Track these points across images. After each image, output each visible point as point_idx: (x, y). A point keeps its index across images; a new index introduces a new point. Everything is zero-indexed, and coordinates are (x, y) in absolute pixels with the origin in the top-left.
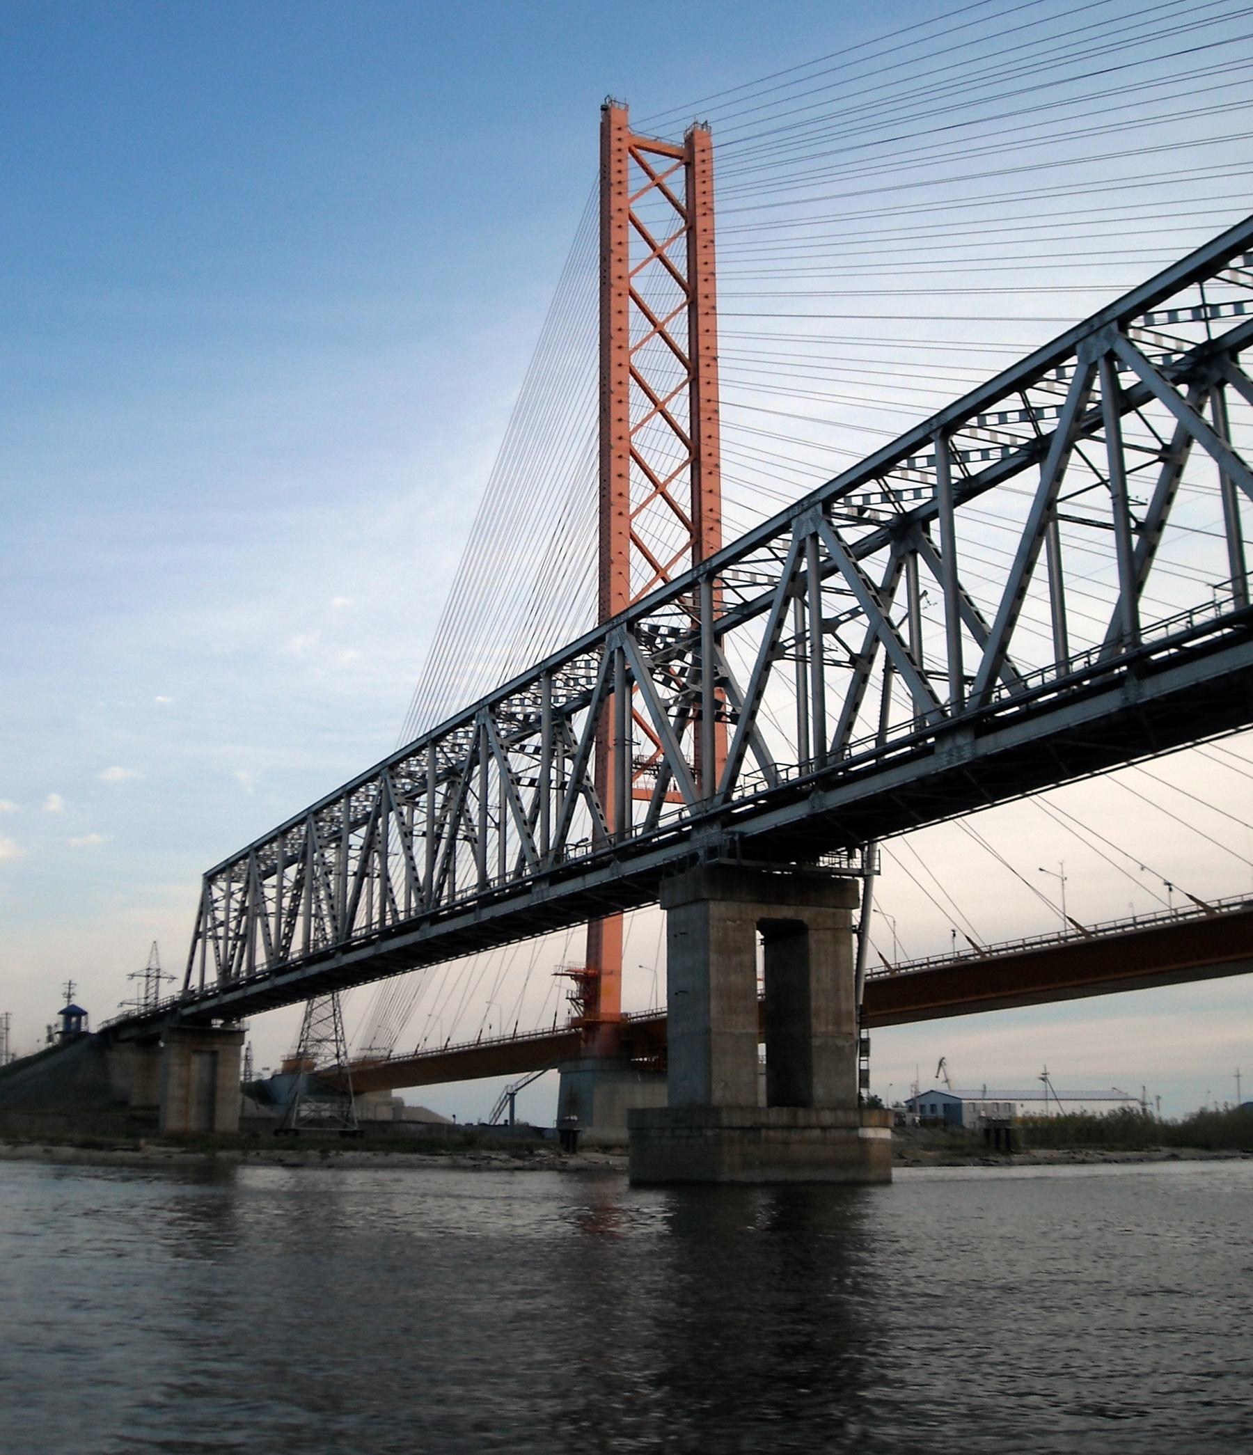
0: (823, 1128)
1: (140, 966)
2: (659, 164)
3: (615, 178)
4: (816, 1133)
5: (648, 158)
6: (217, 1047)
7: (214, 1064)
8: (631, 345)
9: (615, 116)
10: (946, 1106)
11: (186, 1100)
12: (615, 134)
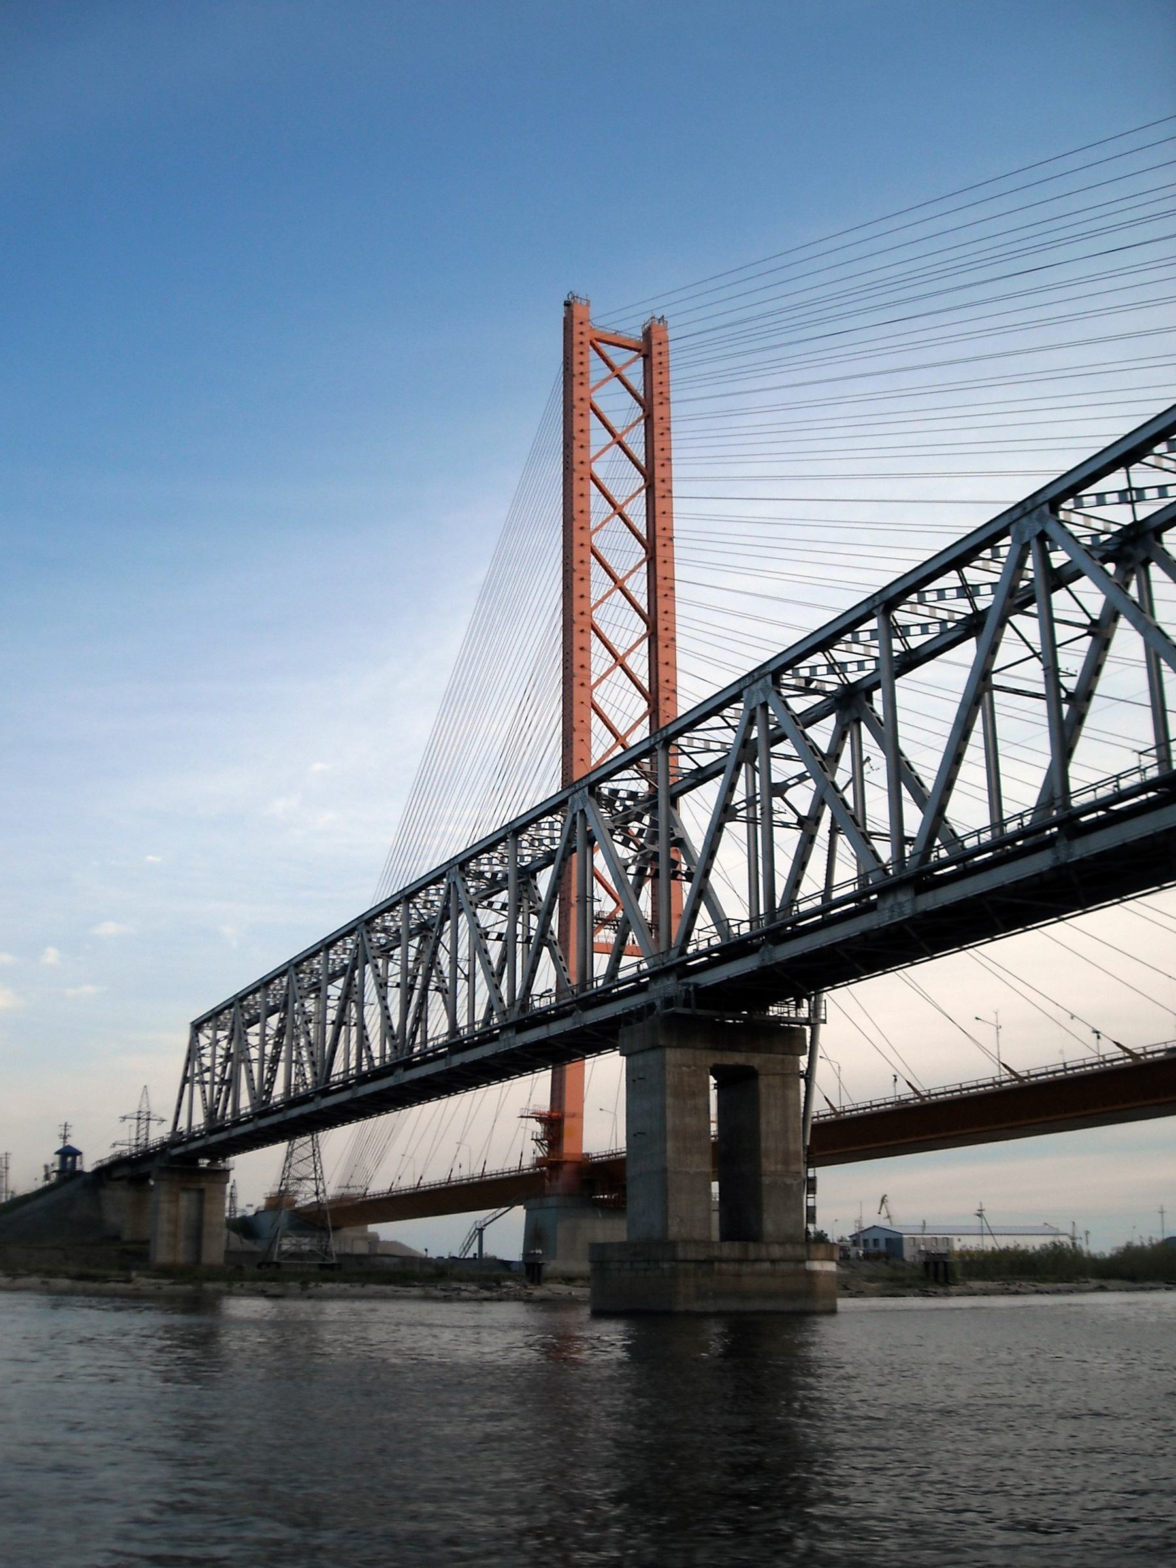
0: (773, 1261)
1: (132, 1109)
2: (619, 357)
4: (766, 1266)
6: (204, 1185)
7: (201, 1202)
8: (593, 526)
10: (888, 1240)
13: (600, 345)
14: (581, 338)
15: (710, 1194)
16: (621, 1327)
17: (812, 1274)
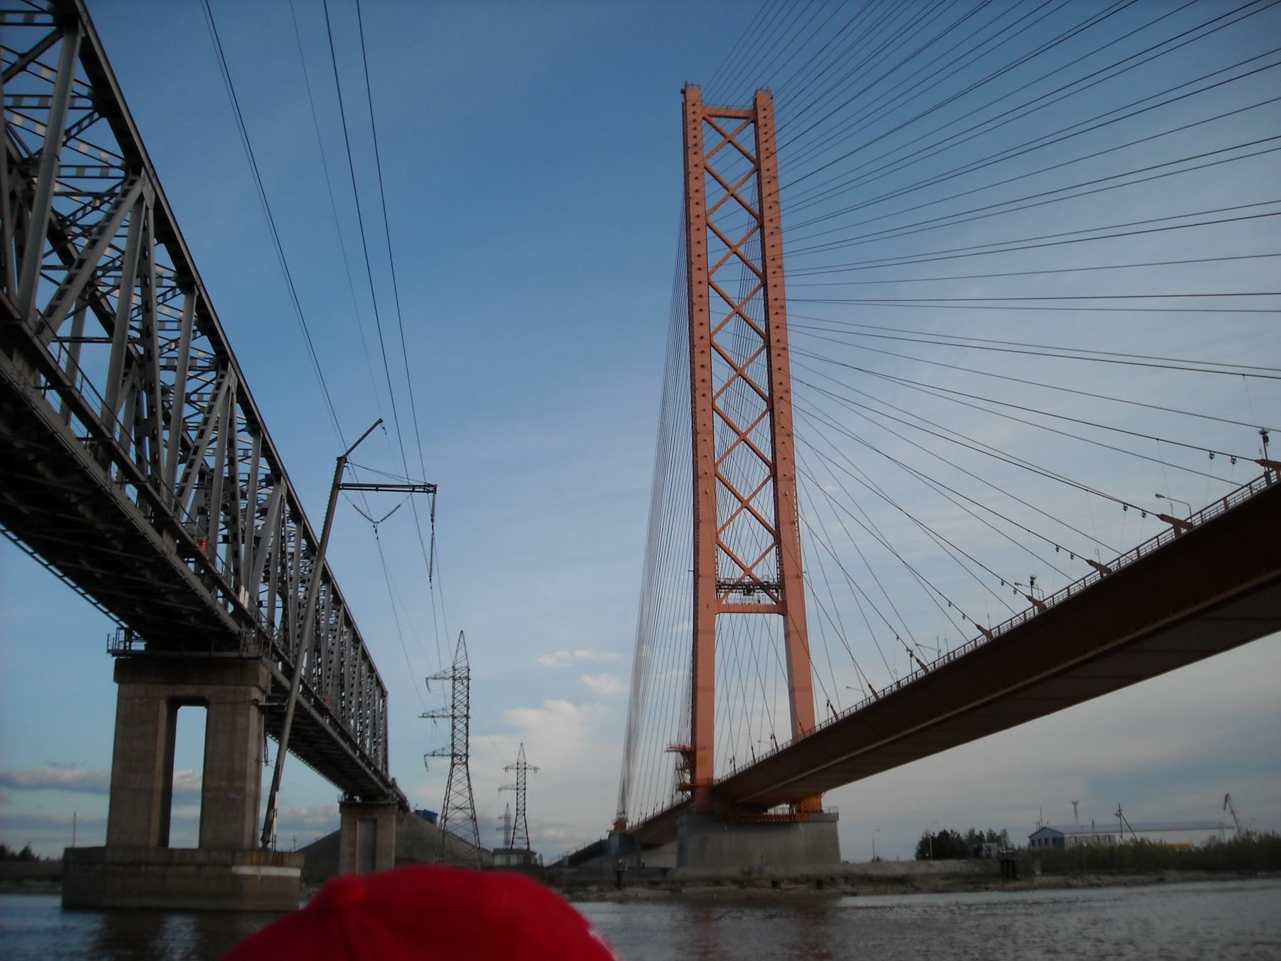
0: (199, 866)
1: (512, 760)
2: (729, 126)
3: (691, 142)
4: (192, 869)
5: (720, 123)
6: (376, 816)
7: (375, 829)
8: (712, 263)
9: (691, 96)
10: (1054, 839)
11: (353, 855)
12: (690, 110)
13: (714, 120)
14: (695, 117)
15: (774, 805)
16: (100, 917)
17: (237, 877)
